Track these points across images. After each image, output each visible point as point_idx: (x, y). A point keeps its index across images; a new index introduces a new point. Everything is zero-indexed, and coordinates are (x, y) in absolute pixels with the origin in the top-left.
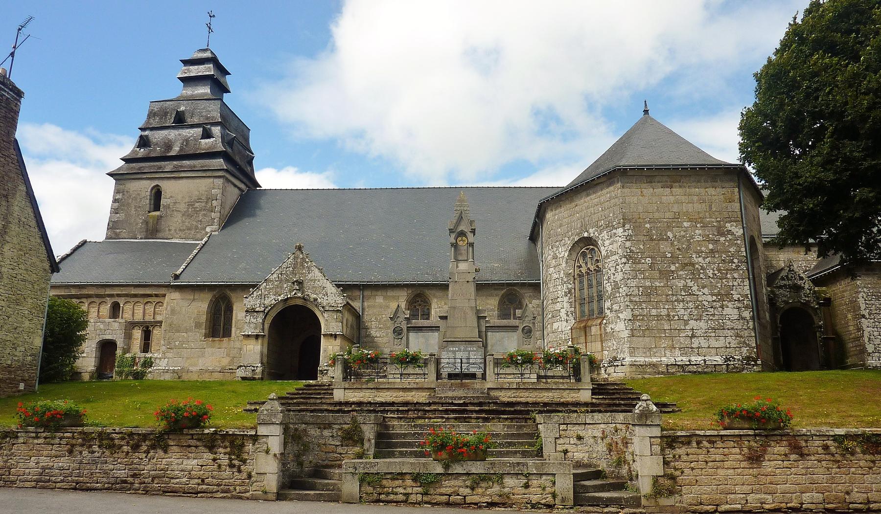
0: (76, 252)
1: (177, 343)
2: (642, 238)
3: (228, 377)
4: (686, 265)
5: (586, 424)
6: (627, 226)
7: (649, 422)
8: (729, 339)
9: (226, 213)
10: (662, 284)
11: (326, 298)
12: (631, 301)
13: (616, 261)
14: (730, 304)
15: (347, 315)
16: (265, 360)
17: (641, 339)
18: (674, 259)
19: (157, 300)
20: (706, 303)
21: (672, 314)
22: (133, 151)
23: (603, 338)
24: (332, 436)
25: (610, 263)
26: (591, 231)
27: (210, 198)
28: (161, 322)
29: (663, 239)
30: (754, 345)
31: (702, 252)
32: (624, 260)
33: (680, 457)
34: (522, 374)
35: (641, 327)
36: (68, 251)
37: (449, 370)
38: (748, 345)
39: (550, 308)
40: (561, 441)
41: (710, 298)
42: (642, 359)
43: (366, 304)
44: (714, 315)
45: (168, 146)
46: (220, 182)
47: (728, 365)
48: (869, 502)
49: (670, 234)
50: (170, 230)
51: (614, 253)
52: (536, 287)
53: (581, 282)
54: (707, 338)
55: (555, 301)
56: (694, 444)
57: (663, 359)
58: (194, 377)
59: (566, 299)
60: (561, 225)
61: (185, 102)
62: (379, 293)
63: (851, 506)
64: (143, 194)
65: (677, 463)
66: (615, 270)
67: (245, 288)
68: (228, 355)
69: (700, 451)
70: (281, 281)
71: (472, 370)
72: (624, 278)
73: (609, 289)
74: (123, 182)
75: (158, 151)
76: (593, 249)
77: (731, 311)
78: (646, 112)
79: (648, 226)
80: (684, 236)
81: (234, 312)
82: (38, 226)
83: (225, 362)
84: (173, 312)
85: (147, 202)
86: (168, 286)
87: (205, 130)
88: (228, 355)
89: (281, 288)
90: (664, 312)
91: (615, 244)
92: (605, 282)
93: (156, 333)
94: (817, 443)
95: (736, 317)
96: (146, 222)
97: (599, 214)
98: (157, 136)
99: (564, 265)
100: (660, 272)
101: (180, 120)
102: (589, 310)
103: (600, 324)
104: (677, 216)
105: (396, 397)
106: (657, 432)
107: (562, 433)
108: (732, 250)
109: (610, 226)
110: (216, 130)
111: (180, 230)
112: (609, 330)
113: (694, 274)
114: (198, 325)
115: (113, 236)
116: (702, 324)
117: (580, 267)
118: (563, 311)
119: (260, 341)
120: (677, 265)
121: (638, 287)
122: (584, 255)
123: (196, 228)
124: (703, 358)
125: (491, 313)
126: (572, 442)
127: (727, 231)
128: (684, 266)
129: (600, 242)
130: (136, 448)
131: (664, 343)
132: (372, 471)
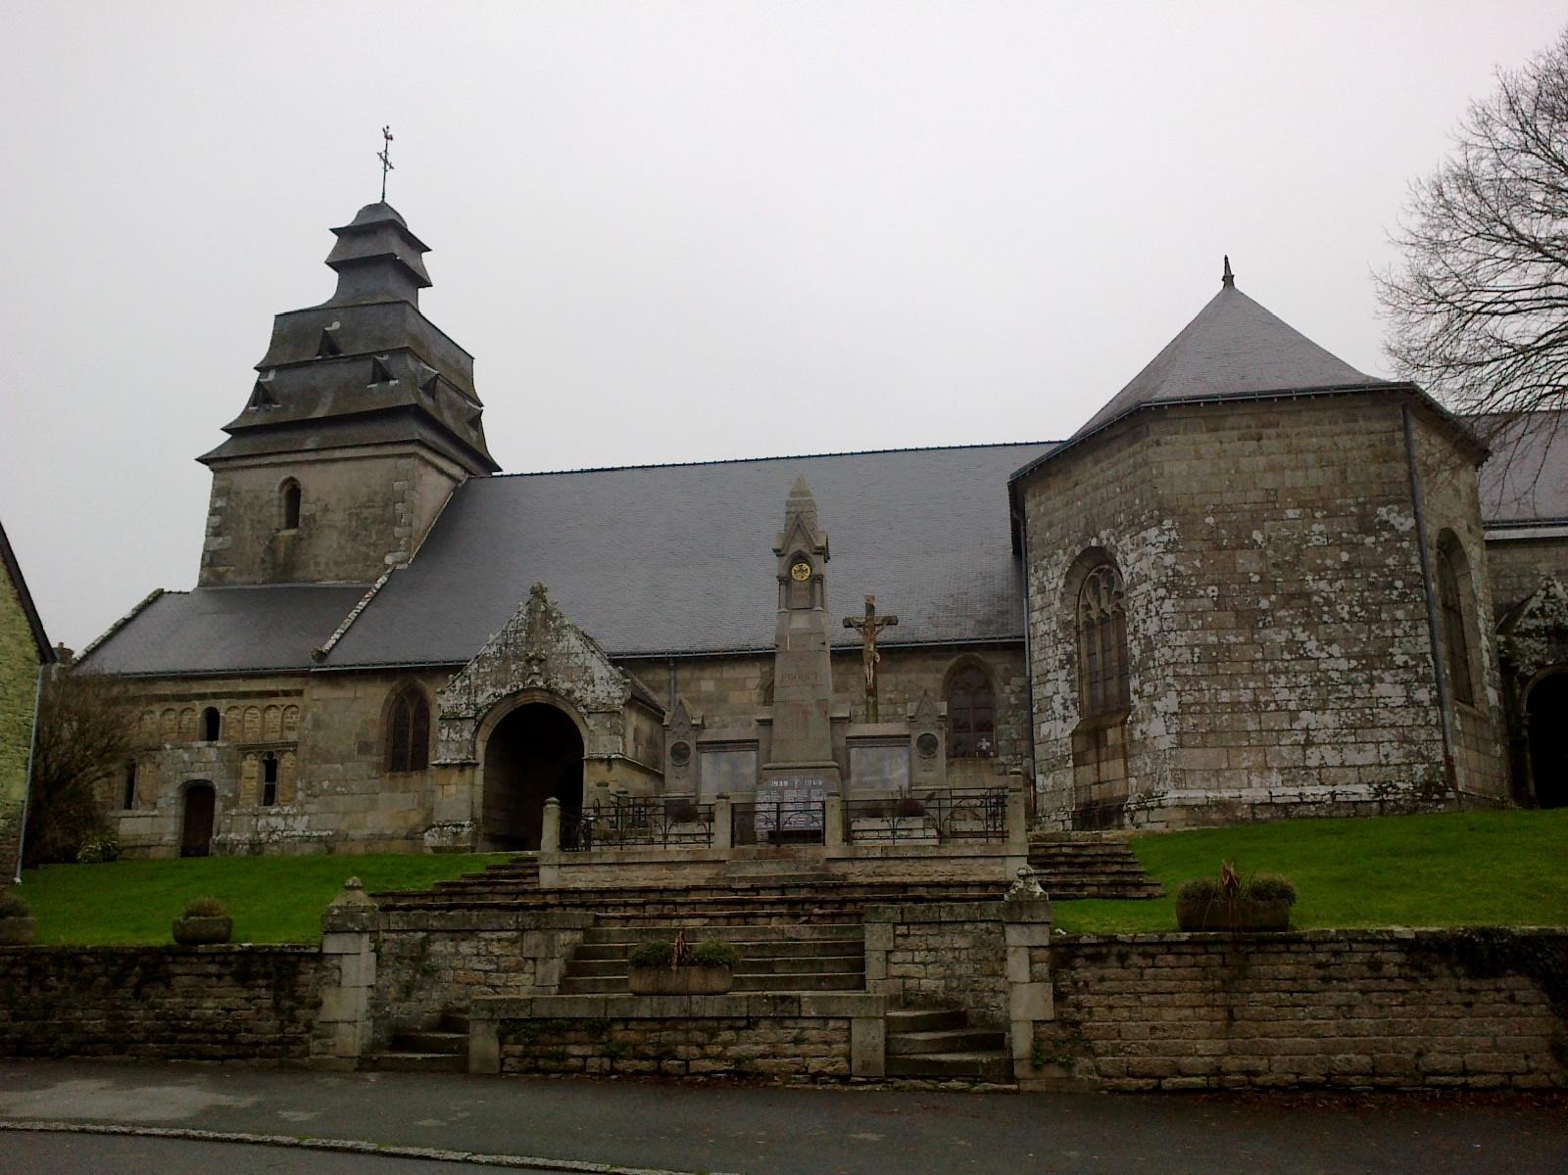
1: (325, 784)
2: (1197, 545)
4: (1292, 596)
5: (940, 923)
6: (1167, 523)
7: (1025, 918)
8: (1386, 748)
9: (423, 527)
10: (1241, 639)
11: (590, 688)
12: (1176, 676)
14: (1387, 676)
16: (479, 813)
17: (1198, 752)
18: (1267, 585)
19: (288, 701)
20: (1335, 675)
21: (1263, 699)
22: (245, 413)
23: (1125, 753)
24: (478, 955)
25: (1137, 599)
26: (1103, 534)
28: (295, 744)
30: (1440, 758)
31: (1327, 568)
32: (1162, 592)
33: (1086, 984)
34: (894, 831)
35: (1202, 728)
36: (126, 612)
38: (1426, 759)
39: (1037, 692)
40: (898, 957)
41: (1343, 665)
42: (1201, 794)
44: (1352, 699)
47: (1382, 802)
48: (1465, 1073)
49: (1257, 536)
53: (1090, 642)
54: (1339, 746)
59: (1062, 674)
60: (1050, 525)
62: (707, 674)
63: (1431, 1079)
65: (1081, 997)
66: (1150, 616)
67: (452, 669)
69: (1126, 973)
70: (505, 659)
72: (1162, 630)
73: (1136, 652)
74: (232, 475)
77: (1389, 690)
78: (1228, 279)
79: (1210, 520)
80: (1287, 539)
82: (12, 579)
84: (317, 725)
85: (276, 513)
86: (304, 674)
89: (507, 670)
90: (1246, 696)
91: (1144, 561)
92: (1130, 638)
93: (286, 762)
94: (1359, 958)
95: (1401, 701)
99: (1057, 604)
104: (1272, 497)
106: (1041, 936)
107: (900, 940)
108: (1390, 561)
109: (1136, 525)
111: (336, 563)
112: (1137, 735)
113: (1308, 615)
114: (364, 748)
116: (1328, 718)
117: (1088, 607)
118: (1058, 699)
119: (468, 772)
120: (1273, 598)
121: (1191, 647)
122: (1095, 583)
123: (367, 557)
124: (1331, 789)
126: (917, 960)
127: (1380, 522)
128: (1287, 600)
129: (1119, 558)
130: (118, 982)
131: (1248, 759)
132: (523, 1015)
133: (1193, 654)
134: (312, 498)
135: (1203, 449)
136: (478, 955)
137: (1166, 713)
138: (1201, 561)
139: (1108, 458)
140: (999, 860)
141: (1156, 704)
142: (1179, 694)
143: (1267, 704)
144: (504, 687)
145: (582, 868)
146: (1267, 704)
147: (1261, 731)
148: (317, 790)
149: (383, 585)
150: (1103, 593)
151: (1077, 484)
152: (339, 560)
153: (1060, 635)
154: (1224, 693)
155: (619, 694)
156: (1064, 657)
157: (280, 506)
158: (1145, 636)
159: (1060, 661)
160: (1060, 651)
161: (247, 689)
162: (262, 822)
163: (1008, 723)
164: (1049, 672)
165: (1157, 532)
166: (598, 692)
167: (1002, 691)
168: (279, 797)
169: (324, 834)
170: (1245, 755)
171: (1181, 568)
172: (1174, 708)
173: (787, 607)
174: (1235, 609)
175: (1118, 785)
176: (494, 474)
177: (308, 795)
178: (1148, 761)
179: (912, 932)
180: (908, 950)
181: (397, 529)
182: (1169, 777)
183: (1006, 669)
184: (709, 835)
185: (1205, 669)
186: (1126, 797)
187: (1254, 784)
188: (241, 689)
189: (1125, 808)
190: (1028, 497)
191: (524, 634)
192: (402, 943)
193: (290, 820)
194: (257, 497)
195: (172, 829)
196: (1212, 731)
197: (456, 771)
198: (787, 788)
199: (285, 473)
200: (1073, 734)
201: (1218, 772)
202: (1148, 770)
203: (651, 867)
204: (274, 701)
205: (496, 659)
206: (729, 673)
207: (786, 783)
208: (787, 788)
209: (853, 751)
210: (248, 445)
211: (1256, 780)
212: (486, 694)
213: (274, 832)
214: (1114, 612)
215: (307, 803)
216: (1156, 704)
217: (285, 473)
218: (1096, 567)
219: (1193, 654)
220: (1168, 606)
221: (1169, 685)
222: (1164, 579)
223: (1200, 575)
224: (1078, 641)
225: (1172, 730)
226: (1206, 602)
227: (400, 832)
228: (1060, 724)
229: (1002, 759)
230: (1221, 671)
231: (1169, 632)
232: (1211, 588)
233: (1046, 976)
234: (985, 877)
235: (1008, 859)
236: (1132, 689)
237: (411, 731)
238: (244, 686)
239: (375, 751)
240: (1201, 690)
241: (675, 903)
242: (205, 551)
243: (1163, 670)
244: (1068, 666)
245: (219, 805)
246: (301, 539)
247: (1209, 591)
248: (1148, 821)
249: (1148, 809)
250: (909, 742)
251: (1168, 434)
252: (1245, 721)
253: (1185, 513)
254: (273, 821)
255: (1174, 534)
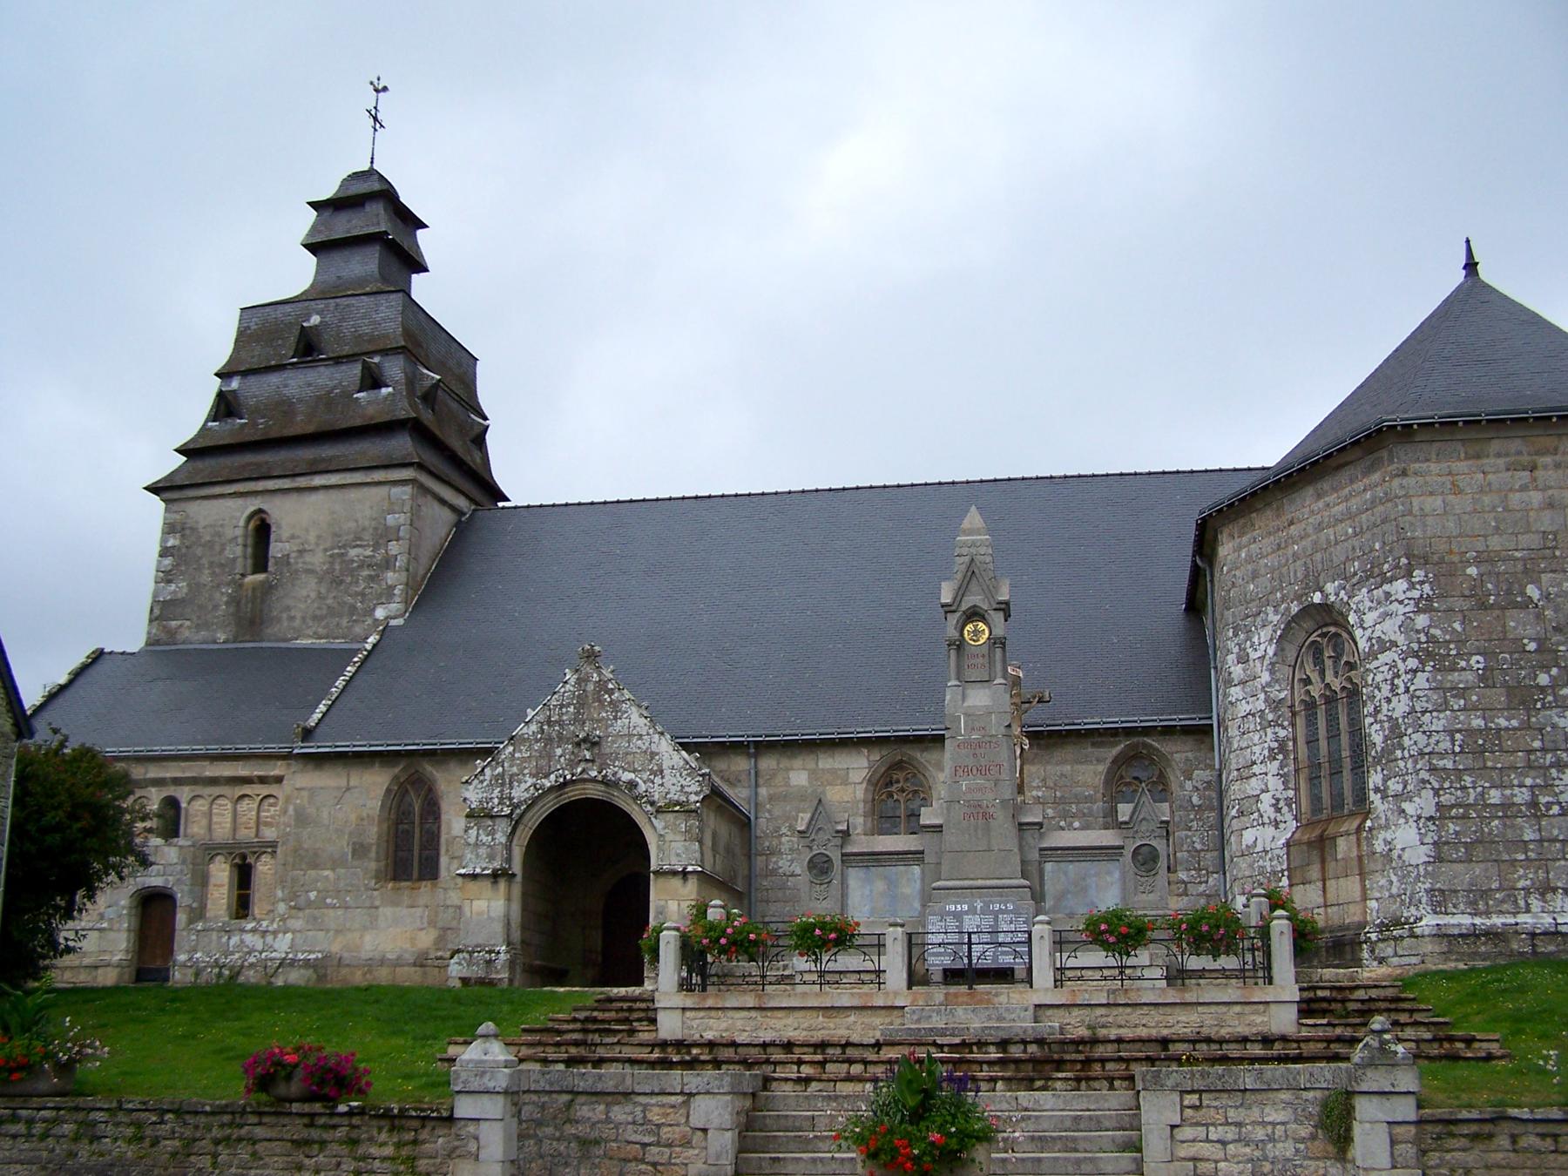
0: (82, 680)
1: (313, 895)
2: (1458, 604)
3: (433, 977)
6: (1418, 574)
9: (421, 572)
10: (1515, 723)
11: (658, 780)
12: (1433, 770)
13: (1393, 666)
15: (712, 820)
16: (516, 935)
17: (1460, 867)
19: (264, 790)
21: (1543, 800)
26: (1330, 588)
27: (385, 535)
28: (273, 845)
29: (1514, 601)
32: (1412, 663)
35: (1463, 839)
37: (947, 961)
39: (1236, 790)
40: (1187, 1132)
42: (1466, 920)
43: (763, 791)
45: (285, 407)
46: (404, 492)
49: (1532, 591)
50: (292, 618)
51: (1385, 645)
52: (1201, 733)
53: (1311, 722)
55: (1245, 774)
56: (1504, 1142)
57: (1521, 918)
58: (358, 978)
59: (1273, 767)
60: (1255, 576)
61: (321, 305)
62: (798, 762)
64: (229, 533)
66: (1394, 693)
68: (432, 923)
70: (549, 740)
71: (1006, 960)
72: (1413, 711)
74: (183, 505)
75: (263, 427)
76: (1337, 635)
78: (1471, 266)
79: (1472, 571)
81: (444, 817)
83: (426, 940)
84: (302, 819)
85: (237, 551)
87: (367, 368)
88: (432, 923)
89: (550, 756)
92: (1369, 720)
93: (264, 868)
96: (235, 601)
97: (1348, 545)
98: (257, 390)
99: (1266, 677)
100: (1510, 691)
101: (308, 348)
102: (1334, 792)
103: (1359, 829)
105: (809, 1029)
107: (1189, 1112)
109: (1375, 576)
110: (394, 368)
111: (315, 618)
112: (1379, 846)
114: (359, 850)
115: (163, 636)
117: (1307, 681)
118: (1266, 799)
119: (502, 884)
120: (1554, 671)
121: (1451, 733)
123: (353, 609)
125: (1085, 807)
126: (1213, 1137)
129: (1352, 618)
133: (1453, 741)
134: (285, 534)
135: (1462, 481)
136: (634, 1123)
137: (1419, 817)
138: (1463, 623)
139: (1335, 490)
140: (1261, 1007)
141: (1405, 805)
142: (1436, 793)
143: (1549, 805)
144: (547, 776)
145: (713, 1013)
146: (1549, 805)
147: (1541, 841)
148: (302, 901)
149: (375, 646)
150: (1329, 663)
151: (1291, 523)
152: (318, 613)
153: (1270, 717)
154: (1493, 792)
155: (695, 788)
156: (1276, 745)
157: (245, 546)
158: (1390, 718)
159: (1271, 750)
160: (1270, 735)
161: (217, 774)
162: (235, 940)
163: (1190, 829)
164: (1254, 763)
165: (1405, 586)
166: (668, 785)
167: (1182, 787)
168: (257, 909)
169: (312, 956)
170: (1521, 872)
171: (1436, 632)
172: (1430, 810)
173: (958, 679)
174: (1505, 685)
175: (1352, 908)
176: (500, 504)
177: (294, 908)
178: (1394, 879)
179: (1205, 1103)
180: (1198, 1124)
181: (390, 574)
182: (1424, 900)
183: (1187, 760)
184: (879, 972)
185: (1469, 761)
186: (1363, 925)
187: (1534, 909)
188: (207, 774)
189: (1363, 938)
190: (1223, 537)
191: (571, 709)
192: (543, 1107)
193: (269, 938)
194: (219, 535)
195: (124, 946)
196: (1479, 841)
197: (487, 884)
198: (966, 913)
199: (253, 505)
200: (1288, 844)
201: (1486, 894)
202: (1394, 891)
203: (802, 1013)
204: (247, 790)
205: (537, 741)
206: (827, 762)
207: (965, 907)
208: (966, 913)
209: (1048, 867)
210: (208, 465)
211: (1536, 904)
212: (523, 786)
213: (249, 953)
214: (1344, 688)
215: (290, 917)
216: (1405, 805)
217: (253, 505)
218: (1319, 631)
219: (1453, 741)
220: (1421, 681)
221: (1423, 781)
222: (1415, 646)
223: (1460, 642)
224: (1293, 725)
225: (1428, 840)
226: (1469, 677)
227: (407, 956)
228: (1270, 830)
229: (1183, 875)
230: (1489, 764)
231: (1423, 713)
232: (1475, 658)
233: (1413, 1162)
234: (1243, 1030)
235: (1272, 1006)
236: (1371, 786)
237: (417, 830)
238: (212, 770)
239: (373, 854)
240: (1464, 788)
241: (865, 1063)
242: (155, 602)
243: (1416, 762)
244: (1280, 757)
245: (181, 918)
246: (271, 587)
247: (1473, 661)
248: (1396, 955)
249: (1395, 939)
250: (1121, 855)
251: (1418, 460)
252: (1521, 828)
253: (1441, 561)
254: (248, 938)
255: (1427, 588)
